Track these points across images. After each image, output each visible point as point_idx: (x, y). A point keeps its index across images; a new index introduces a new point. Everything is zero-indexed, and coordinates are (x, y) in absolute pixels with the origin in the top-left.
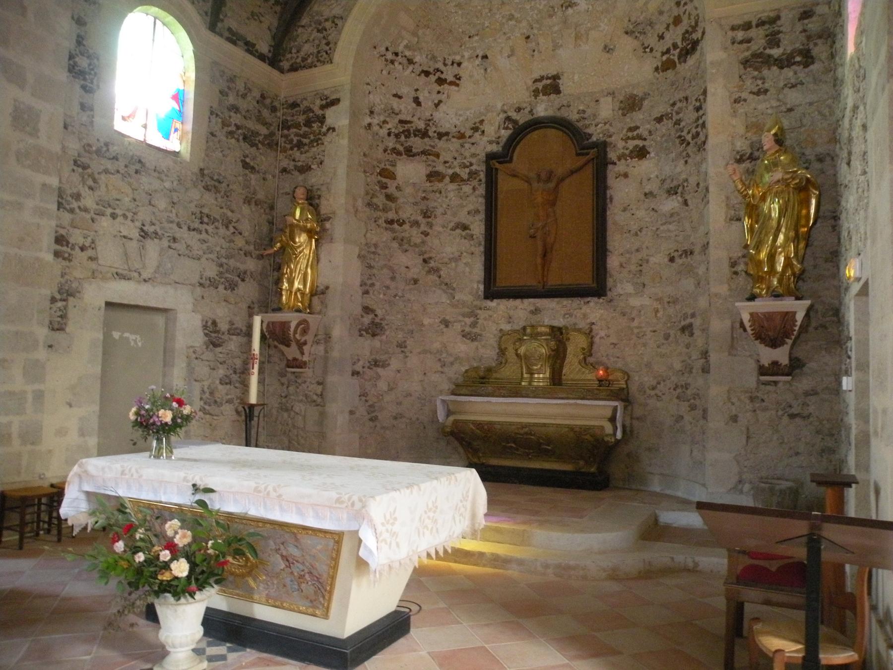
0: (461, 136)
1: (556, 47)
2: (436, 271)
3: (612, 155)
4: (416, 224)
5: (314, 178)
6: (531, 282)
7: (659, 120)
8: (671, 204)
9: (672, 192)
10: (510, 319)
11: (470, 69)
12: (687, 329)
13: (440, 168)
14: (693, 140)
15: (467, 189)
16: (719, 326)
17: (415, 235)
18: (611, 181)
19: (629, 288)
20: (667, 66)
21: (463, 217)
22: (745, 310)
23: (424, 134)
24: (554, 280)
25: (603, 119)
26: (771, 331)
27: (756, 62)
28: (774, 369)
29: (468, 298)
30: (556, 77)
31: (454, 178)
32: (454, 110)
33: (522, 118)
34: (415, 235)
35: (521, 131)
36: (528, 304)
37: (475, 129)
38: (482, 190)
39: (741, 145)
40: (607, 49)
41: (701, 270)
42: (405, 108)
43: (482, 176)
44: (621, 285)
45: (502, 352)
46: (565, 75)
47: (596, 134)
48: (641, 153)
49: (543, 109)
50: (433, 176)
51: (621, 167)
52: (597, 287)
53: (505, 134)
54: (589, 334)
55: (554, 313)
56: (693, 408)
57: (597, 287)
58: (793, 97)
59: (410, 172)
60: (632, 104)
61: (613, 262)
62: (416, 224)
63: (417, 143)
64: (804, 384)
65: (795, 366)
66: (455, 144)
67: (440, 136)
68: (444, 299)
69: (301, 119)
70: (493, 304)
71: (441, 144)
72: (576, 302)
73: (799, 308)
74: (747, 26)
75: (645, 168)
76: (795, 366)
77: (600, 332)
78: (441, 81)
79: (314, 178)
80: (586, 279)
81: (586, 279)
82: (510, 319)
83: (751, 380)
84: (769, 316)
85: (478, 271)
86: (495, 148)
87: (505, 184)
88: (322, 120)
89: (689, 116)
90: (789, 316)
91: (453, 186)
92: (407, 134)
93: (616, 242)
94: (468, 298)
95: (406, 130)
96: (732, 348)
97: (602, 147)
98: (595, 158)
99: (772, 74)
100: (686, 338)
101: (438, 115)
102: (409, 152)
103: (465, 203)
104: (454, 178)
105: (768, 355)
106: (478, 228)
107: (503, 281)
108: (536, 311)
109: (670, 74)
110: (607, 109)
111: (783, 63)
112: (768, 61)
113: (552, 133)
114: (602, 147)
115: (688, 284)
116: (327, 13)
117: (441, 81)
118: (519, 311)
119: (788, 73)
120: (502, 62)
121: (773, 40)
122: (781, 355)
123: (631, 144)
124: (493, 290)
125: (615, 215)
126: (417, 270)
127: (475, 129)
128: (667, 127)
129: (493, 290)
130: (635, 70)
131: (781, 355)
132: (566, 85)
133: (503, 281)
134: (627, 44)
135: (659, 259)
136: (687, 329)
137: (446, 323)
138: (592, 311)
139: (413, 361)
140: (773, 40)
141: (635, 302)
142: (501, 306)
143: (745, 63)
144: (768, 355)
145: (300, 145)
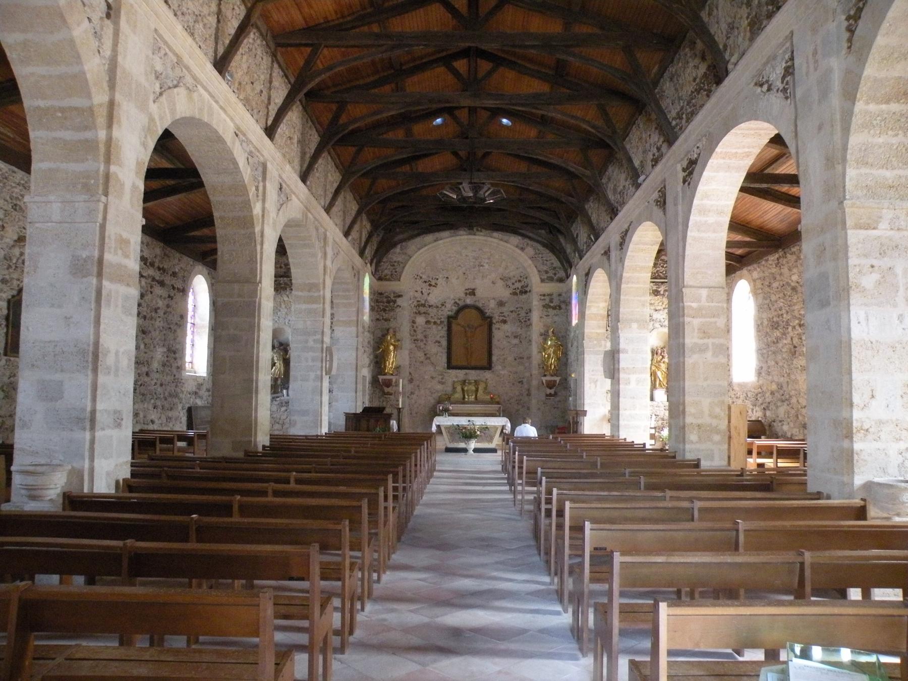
0: (437, 307)
1: (474, 278)
2: (429, 358)
3: (494, 321)
4: (422, 340)
5: (392, 324)
6: (464, 364)
7: (512, 312)
8: (516, 341)
9: (516, 337)
10: (457, 377)
11: (441, 281)
12: (521, 382)
13: (430, 319)
14: (526, 323)
15: (440, 328)
16: (535, 383)
17: (422, 344)
18: (494, 330)
19: (500, 367)
20: (515, 294)
21: (438, 338)
22: (544, 379)
23: (424, 305)
24: (473, 363)
25: (491, 308)
26: (551, 385)
27: (546, 306)
28: (550, 395)
29: (441, 369)
30: (474, 290)
31: (435, 323)
32: (435, 297)
33: (461, 303)
34: (422, 344)
35: (462, 308)
36: (464, 371)
37: (443, 305)
38: (446, 328)
39: (542, 331)
40: (493, 283)
41: (527, 364)
42: (418, 295)
43: (446, 323)
44: (497, 367)
45: (454, 388)
46: (605, 390)
47: (488, 312)
48: (505, 322)
49: (469, 301)
50: (428, 322)
51: (497, 326)
52: (489, 366)
53: (455, 308)
54: (486, 383)
55: (473, 375)
56: (523, 406)
57: (489, 366)
58: (556, 318)
59: (420, 320)
60: (501, 304)
61: (494, 358)
62: (422, 340)
63: (422, 309)
64: (558, 399)
65: (555, 394)
66: (435, 310)
67: (430, 306)
68: (432, 369)
69: (385, 300)
70: (450, 371)
71: (430, 310)
72: (482, 371)
73: (558, 379)
74: (544, 295)
75: (506, 327)
76: (555, 394)
77: (490, 382)
78: (430, 285)
79: (392, 324)
80: (484, 363)
81: (484, 363)
82: (457, 377)
83: (544, 398)
84: (551, 381)
85: (445, 359)
86: (450, 313)
87: (455, 327)
88: (395, 302)
89: (523, 314)
90: (555, 381)
91: (434, 326)
92: (419, 305)
93: (496, 352)
94: (441, 369)
95: (420, 305)
96: (538, 389)
97: (491, 318)
98: (487, 321)
99: (550, 310)
100: (520, 385)
101: (429, 298)
102: (420, 313)
103: (439, 333)
104: (435, 323)
105: (549, 391)
106: (444, 343)
107: (454, 363)
108: (466, 374)
109: (516, 297)
110: (492, 304)
111: (554, 308)
112: (550, 307)
113: (474, 311)
114: (491, 318)
115: (521, 368)
116: (395, 259)
117: (430, 285)
118: (460, 374)
119: (555, 311)
120: (454, 281)
121: (551, 301)
122: (552, 391)
123: (501, 318)
124: (450, 366)
125: (495, 342)
126: (422, 359)
127: (443, 305)
128: (514, 315)
129: (450, 366)
130: (503, 293)
131: (552, 391)
132: (478, 293)
133: (454, 363)
134: (500, 283)
135: (510, 358)
136: (521, 382)
137: (432, 378)
138: (487, 375)
139: (422, 392)
140: (551, 301)
141: (502, 372)
142: (453, 372)
143: (544, 306)
144: (549, 391)
145: (384, 310)
